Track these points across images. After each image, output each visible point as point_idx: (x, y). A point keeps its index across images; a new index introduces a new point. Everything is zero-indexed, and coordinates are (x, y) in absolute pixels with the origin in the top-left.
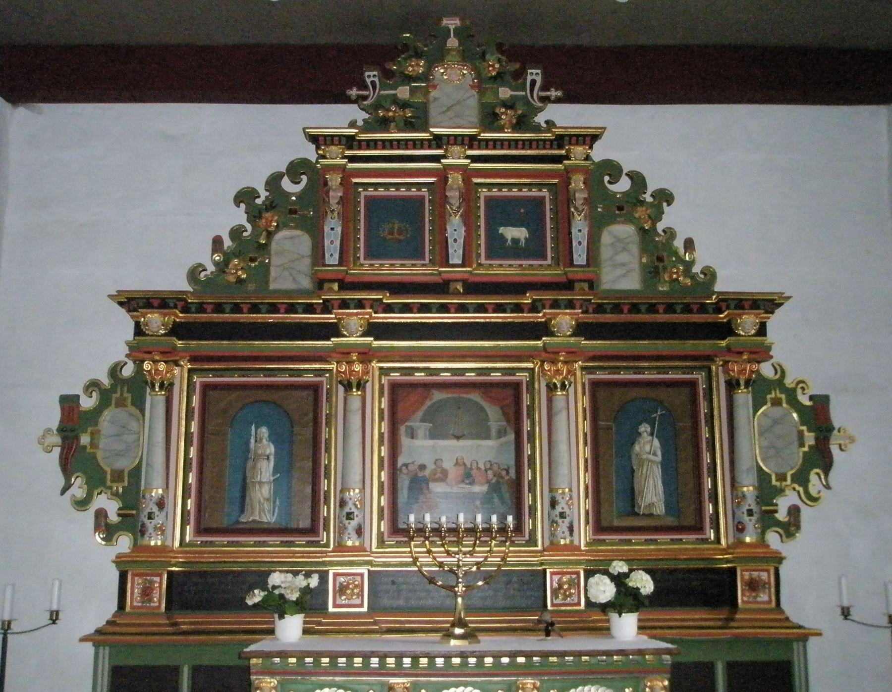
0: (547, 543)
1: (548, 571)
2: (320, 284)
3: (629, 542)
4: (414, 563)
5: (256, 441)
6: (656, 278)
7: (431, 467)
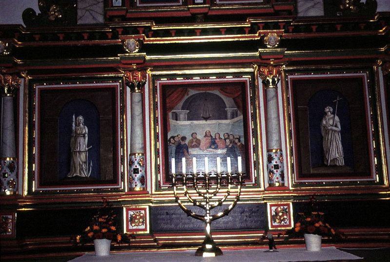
0: (267, 185)
1: (268, 204)
2: (109, 19)
3: (321, 184)
4: (176, 201)
5: (76, 125)
6: (110, 16)
7: (189, 138)
